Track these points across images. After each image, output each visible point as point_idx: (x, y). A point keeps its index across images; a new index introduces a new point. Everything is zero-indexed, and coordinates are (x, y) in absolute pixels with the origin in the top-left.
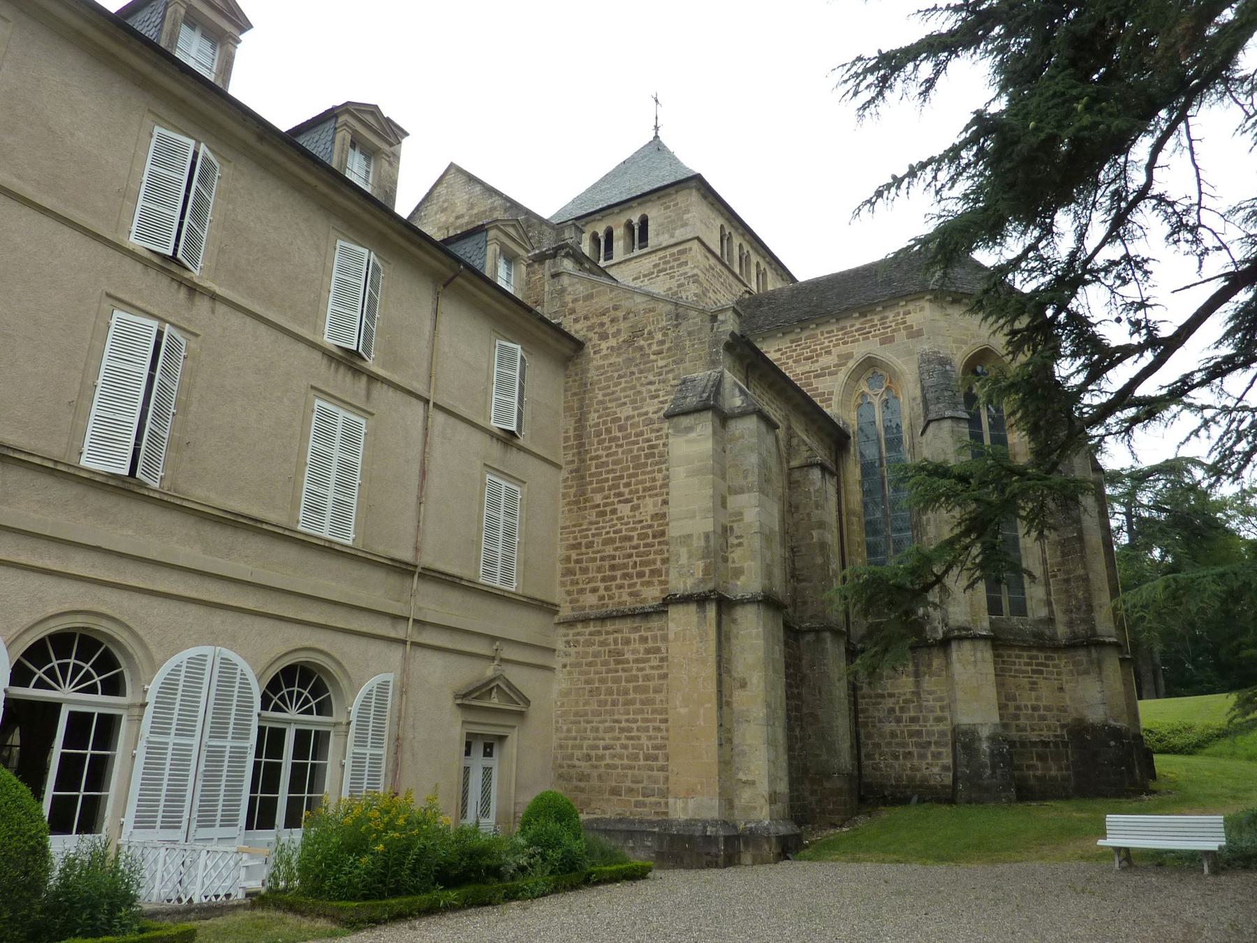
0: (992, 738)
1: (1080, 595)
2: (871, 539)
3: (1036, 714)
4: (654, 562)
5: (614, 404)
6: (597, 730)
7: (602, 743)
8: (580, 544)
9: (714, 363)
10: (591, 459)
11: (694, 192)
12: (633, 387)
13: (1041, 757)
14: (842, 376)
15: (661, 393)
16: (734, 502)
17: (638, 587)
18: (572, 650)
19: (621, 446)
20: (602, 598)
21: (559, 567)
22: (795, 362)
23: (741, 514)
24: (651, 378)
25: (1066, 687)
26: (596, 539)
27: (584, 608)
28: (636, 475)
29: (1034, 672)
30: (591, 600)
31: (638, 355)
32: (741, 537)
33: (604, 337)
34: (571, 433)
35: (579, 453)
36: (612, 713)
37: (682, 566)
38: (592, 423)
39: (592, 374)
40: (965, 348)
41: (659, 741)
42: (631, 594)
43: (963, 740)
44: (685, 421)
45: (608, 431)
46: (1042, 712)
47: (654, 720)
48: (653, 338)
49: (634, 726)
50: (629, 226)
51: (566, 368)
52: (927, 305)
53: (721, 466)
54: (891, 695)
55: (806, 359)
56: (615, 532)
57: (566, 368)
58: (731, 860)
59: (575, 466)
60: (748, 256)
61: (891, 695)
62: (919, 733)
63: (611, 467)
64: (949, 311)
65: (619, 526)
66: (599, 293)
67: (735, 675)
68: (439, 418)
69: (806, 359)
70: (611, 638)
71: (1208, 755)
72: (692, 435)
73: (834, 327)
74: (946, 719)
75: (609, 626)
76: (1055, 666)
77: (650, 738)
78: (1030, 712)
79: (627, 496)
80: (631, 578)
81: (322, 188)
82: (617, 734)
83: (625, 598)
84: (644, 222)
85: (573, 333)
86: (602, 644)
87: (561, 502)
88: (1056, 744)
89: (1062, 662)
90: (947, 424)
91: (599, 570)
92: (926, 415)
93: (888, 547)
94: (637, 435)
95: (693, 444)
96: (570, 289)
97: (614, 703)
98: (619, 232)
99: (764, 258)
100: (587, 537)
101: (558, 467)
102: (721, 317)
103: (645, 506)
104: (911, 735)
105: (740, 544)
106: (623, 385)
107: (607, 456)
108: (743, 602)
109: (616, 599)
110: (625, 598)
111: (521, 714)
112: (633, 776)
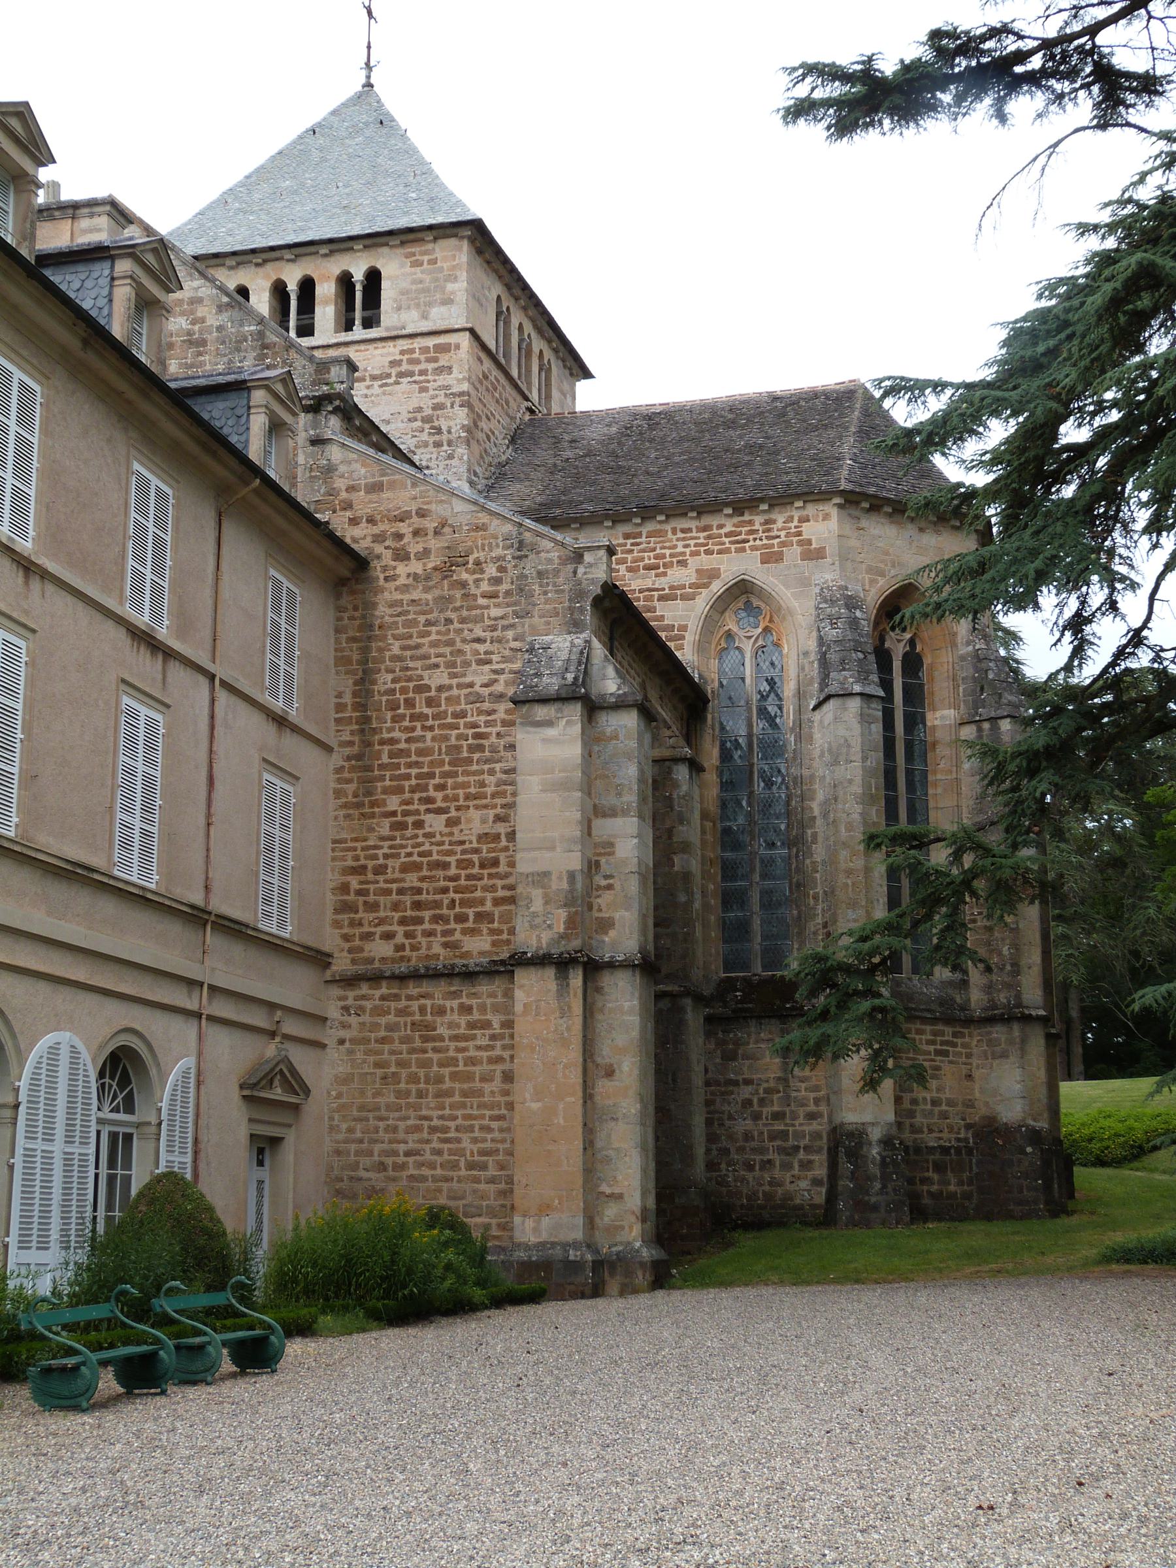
0: (887, 1142)
1: (1005, 950)
2: (728, 854)
3: (937, 1109)
4: (482, 902)
5: (419, 664)
6: (395, 1129)
7: (402, 1148)
8: (364, 867)
9: (575, 626)
10: (382, 742)
11: (465, 244)
12: (450, 643)
13: (939, 1168)
14: (702, 602)
15: (495, 658)
16: (605, 827)
17: (458, 936)
18: (353, 1020)
19: (431, 728)
20: (400, 948)
21: (330, 899)
22: (630, 569)
23: (612, 845)
24: (479, 632)
25: (977, 1074)
26: (390, 862)
27: (371, 961)
28: (454, 774)
29: (938, 1053)
30: (381, 949)
31: (458, 594)
32: (611, 877)
33: (402, 556)
34: (348, 699)
35: (362, 731)
36: (417, 1107)
37: (535, 915)
38: (383, 688)
39: (383, 612)
40: (881, 582)
41: (488, 1145)
42: (446, 945)
43: (844, 1143)
44: (541, 712)
45: (410, 703)
46: (944, 1107)
47: (483, 1117)
48: (482, 572)
49: (452, 1124)
50: (345, 281)
51: (338, 596)
52: (834, 512)
53: (592, 775)
54: (748, 1082)
55: (649, 568)
56: (420, 855)
57: (338, 596)
58: (596, 1291)
59: (356, 749)
60: (530, 345)
61: (748, 1082)
62: (784, 1135)
63: (414, 758)
64: (864, 523)
65: (427, 847)
66: (392, 485)
67: (599, 1060)
68: (222, 696)
69: (649, 568)
70: (415, 1005)
71: (938, 386)
72: (551, 732)
73: (693, 524)
74: (821, 1115)
75: (413, 989)
76: (964, 1046)
77: (475, 1140)
78: (929, 1107)
79: (440, 804)
80: (447, 922)
81: (132, 394)
82: (425, 1135)
83: (437, 949)
84: (374, 278)
85: (348, 540)
86: (402, 1012)
87: (332, 803)
88: (958, 1151)
89: (974, 1039)
90: (855, 704)
91: (396, 907)
92: (824, 684)
93: (753, 870)
94: (456, 715)
95: (551, 747)
96: (342, 468)
97: (421, 1094)
98: (326, 290)
99: (549, 341)
100: (375, 857)
101: (328, 749)
102: (588, 557)
103: (469, 821)
104: (773, 1137)
105: (609, 887)
106: (434, 637)
107: (408, 741)
108: (612, 965)
109: (423, 951)
110: (437, 949)
111: (296, 1108)
112: (450, 1190)
